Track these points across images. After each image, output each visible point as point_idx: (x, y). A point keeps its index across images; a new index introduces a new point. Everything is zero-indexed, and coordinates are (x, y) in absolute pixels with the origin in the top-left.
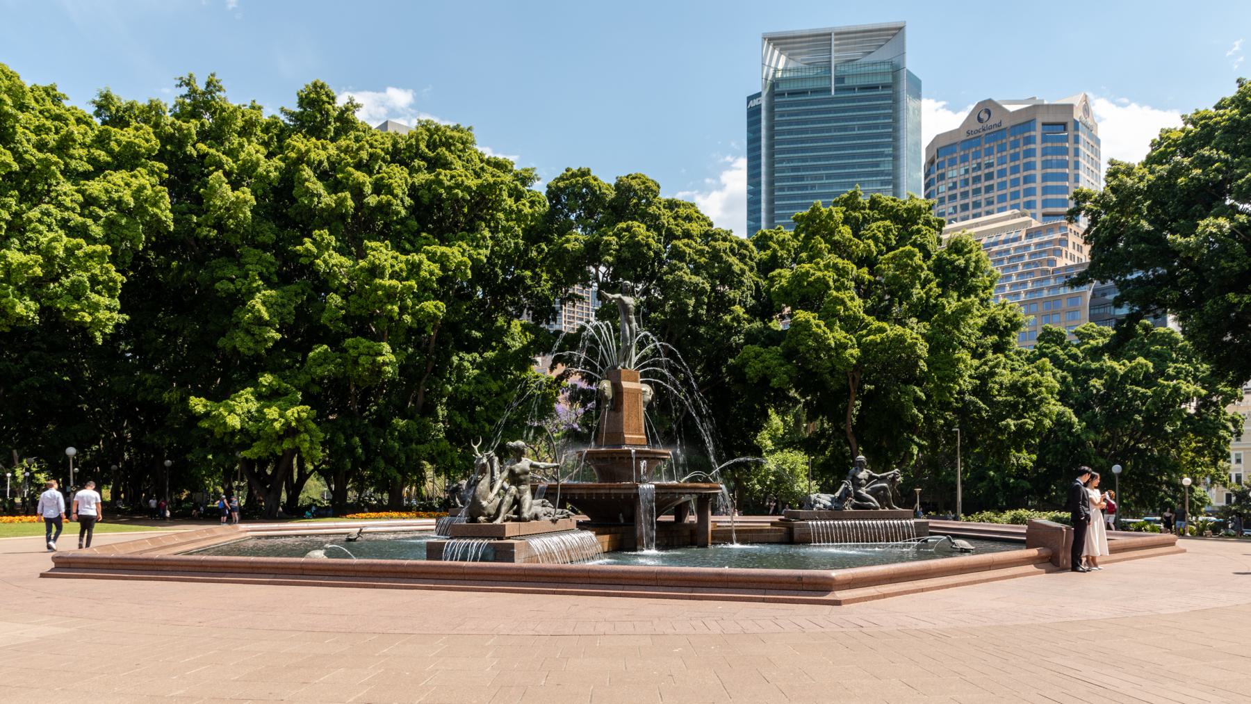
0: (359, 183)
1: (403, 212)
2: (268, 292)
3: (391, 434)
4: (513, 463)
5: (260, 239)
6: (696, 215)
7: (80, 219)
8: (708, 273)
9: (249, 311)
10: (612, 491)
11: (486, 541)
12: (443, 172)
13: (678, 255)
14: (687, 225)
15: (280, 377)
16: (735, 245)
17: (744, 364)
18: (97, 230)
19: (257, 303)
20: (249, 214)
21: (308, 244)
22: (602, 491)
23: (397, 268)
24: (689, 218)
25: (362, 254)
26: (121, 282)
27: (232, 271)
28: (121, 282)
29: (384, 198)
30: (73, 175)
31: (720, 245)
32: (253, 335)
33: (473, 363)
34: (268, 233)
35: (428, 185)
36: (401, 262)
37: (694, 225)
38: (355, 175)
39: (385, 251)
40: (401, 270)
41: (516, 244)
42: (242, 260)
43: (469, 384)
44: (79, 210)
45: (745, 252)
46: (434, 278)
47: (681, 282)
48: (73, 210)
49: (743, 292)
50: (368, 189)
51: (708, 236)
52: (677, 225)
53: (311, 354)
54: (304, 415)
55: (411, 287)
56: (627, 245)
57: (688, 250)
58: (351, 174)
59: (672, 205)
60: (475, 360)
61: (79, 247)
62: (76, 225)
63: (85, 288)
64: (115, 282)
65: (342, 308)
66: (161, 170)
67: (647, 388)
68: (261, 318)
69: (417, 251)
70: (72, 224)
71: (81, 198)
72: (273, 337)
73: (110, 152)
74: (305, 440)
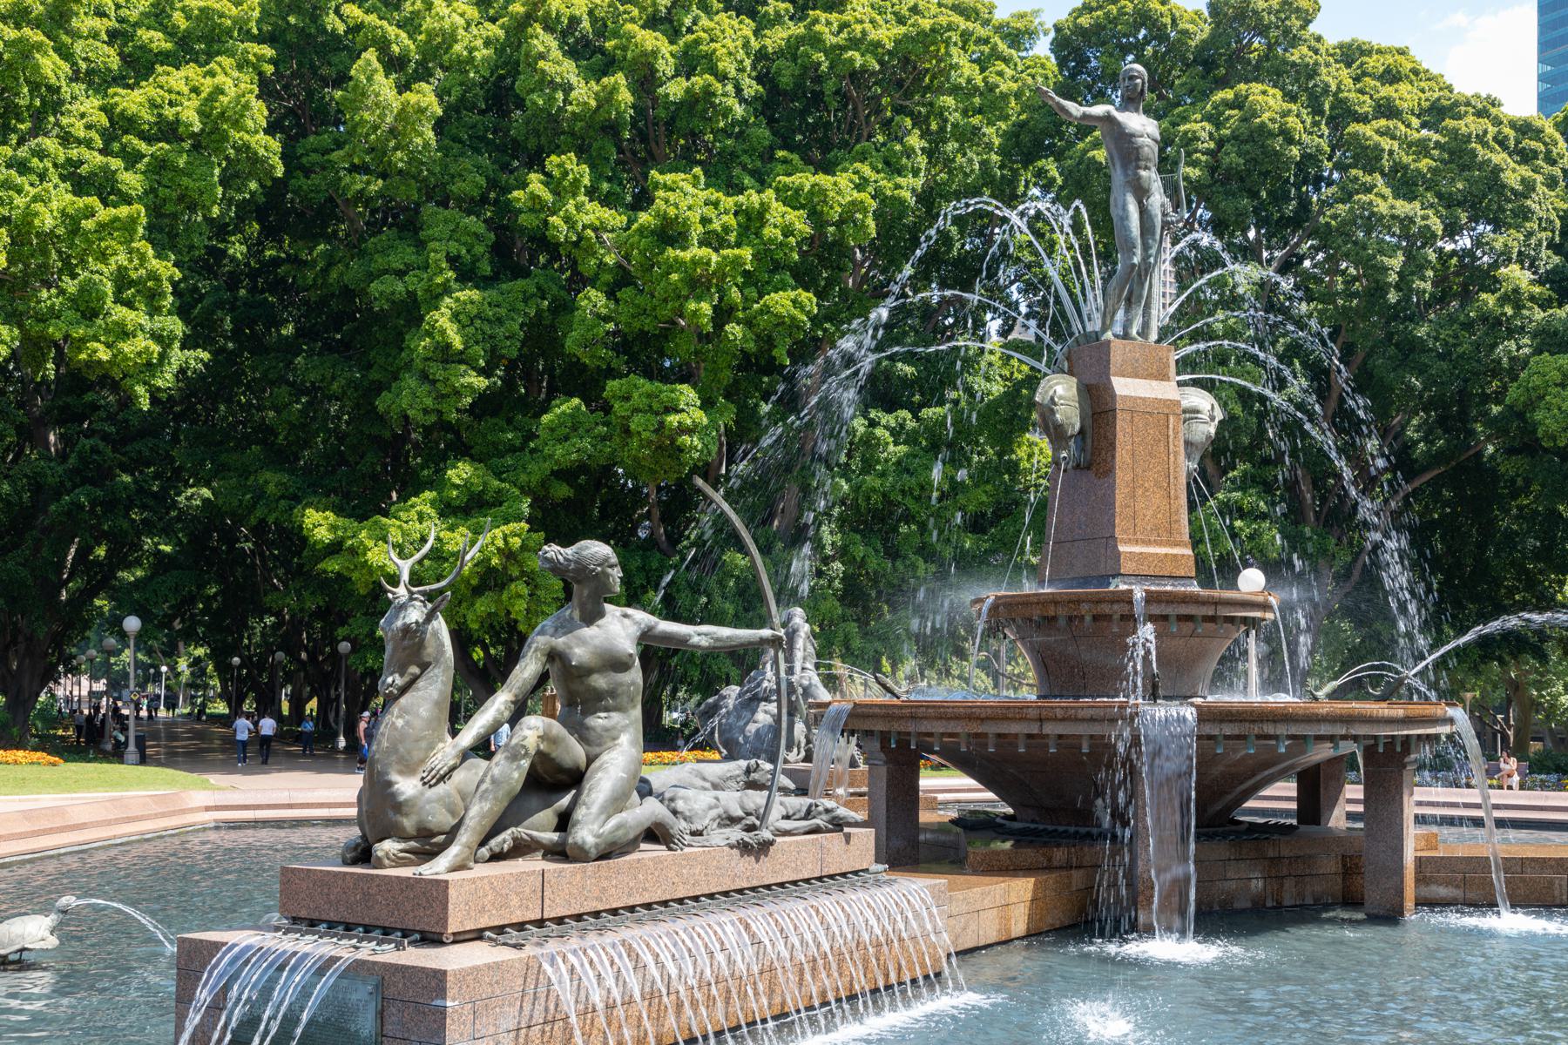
0: (644, 54)
1: (739, 110)
2: (464, 295)
3: (722, 584)
4: (566, 627)
5: (457, 187)
6: (1409, 66)
7: (99, 159)
8: (1439, 195)
9: (429, 334)
10: (1049, 729)
11: (345, 950)
12: (823, 16)
13: (1368, 158)
14: (1386, 91)
15: (489, 467)
16: (1507, 131)
17: (1535, 399)
18: (132, 181)
19: (442, 319)
20: (430, 134)
21: (535, 183)
22: (1015, 728)
23: (716, 226)
24: (1391, 76)
25: (643, 200)
26: (171, 279)
27: (403, 254)
28: (171, 279)
29: (698, 81)
30: (97, 80)
31: (1469, 125)
32: (434, 382)
33: (897, 432)
34: (471, 177)
35: (791, 50)
36: (726, 212)
37: (1404, 87)
38: (639, 37)
39: (689, 188)
40: (726, 229)
41: (983, 163)
42: (422, 234)
43: (883, 475)
44: (99, 143)
45: (1534, 144)
46: (792, 240)
47: (1372, 221)
48: (88, 143)
49: (1530, 235)
50: (665, 66)
51: (1437, 112)
52: (1362, 92)
53: (546, 418)
54: (516, 542)
55: (737, 262)
56: (1235, 137)
57: (1386, 143)
58: (630, 37)
59: (1350, 54)
60: (902, 426)
61: (90, 213)
62: (93, 174)
63: (101, 298)
64: (157, 278)
65: (606, 319)
66: (260, 58)
67: (1202, 400)
68: (449, 346)
69: (762, 183)
70: (84, 170)
71: (105, 121)
72: (470, 386)
73: (170, 33)
74: (520, 596)
